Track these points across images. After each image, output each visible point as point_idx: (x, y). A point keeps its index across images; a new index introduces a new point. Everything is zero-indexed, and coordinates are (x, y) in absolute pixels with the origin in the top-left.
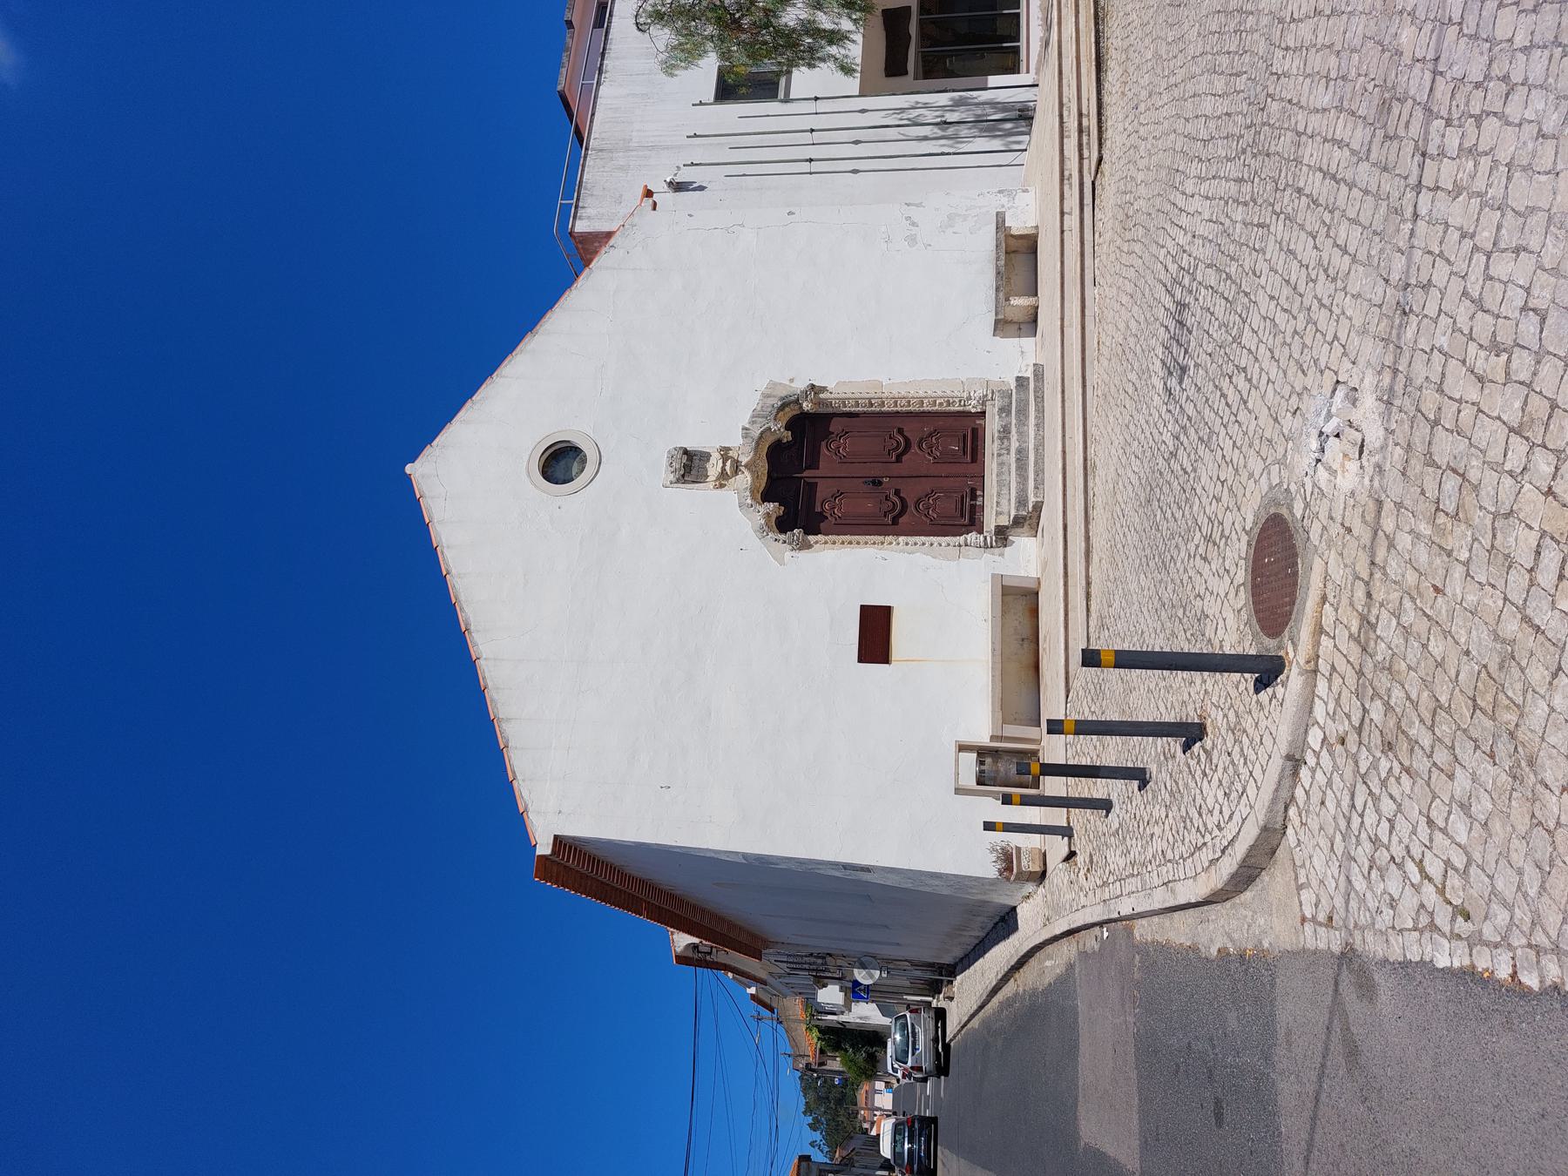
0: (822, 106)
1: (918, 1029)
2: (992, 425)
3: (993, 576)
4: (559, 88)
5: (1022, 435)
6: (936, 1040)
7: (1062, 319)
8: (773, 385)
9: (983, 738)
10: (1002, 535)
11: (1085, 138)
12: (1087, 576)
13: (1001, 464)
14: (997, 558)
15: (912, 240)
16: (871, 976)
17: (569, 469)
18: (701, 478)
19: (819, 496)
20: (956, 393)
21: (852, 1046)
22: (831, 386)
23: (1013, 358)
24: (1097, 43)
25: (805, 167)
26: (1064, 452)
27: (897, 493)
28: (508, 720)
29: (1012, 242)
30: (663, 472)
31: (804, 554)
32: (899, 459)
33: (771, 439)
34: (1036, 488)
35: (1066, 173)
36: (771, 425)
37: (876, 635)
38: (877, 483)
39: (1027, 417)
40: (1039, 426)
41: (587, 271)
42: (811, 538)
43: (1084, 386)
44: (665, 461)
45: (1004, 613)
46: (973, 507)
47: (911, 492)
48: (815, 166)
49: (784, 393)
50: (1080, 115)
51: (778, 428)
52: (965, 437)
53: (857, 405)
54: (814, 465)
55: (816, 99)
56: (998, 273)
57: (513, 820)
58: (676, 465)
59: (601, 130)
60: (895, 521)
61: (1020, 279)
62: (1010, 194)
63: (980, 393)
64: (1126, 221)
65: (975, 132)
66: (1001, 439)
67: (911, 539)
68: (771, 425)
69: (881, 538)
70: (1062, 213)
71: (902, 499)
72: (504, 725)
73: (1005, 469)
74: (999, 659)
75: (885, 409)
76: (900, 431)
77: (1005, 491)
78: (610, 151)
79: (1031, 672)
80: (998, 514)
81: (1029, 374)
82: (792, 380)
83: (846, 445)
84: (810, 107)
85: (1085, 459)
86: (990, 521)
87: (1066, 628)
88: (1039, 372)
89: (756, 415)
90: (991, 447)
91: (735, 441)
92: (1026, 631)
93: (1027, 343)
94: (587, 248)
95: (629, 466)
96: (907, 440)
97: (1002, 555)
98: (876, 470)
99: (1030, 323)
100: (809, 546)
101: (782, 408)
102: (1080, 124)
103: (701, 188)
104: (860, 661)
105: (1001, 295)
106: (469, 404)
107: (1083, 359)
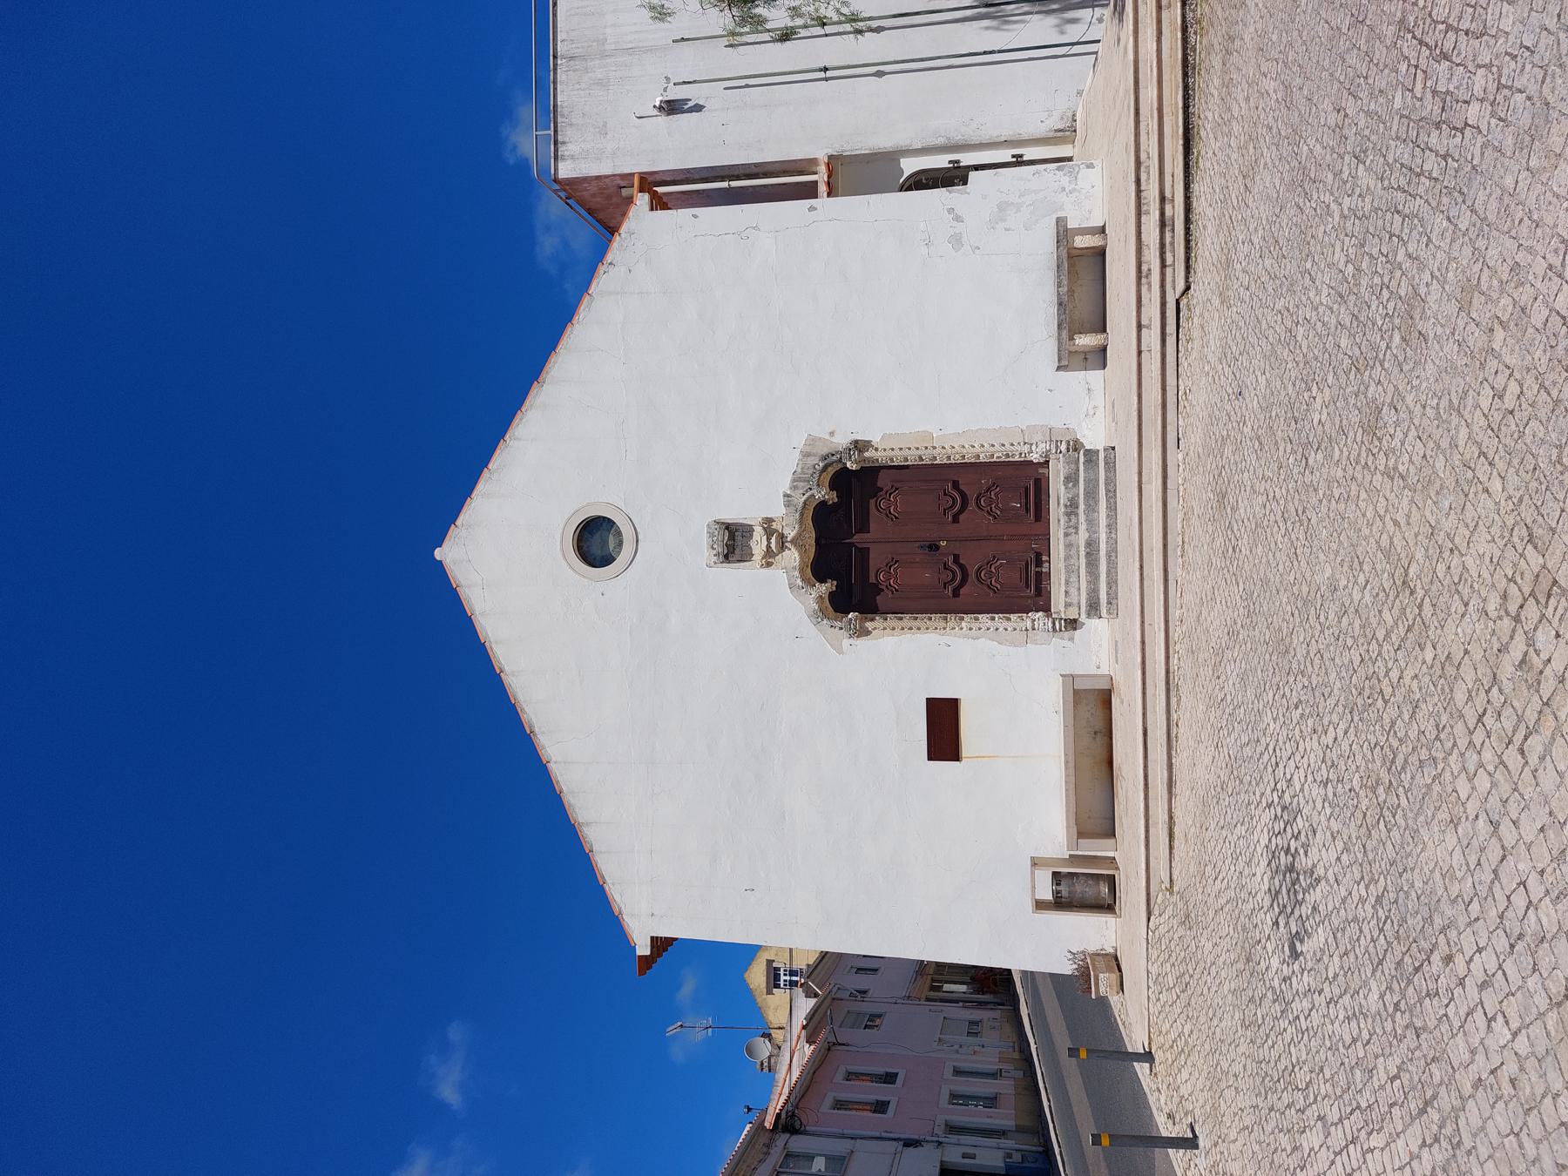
7: (1140, 474)
8: (812, 440)
11: (1168, 235)
13: (1069, 546)
18: (746, 557)
22: (875, 438)
24: (1186, 107)
26: (1143, 642)
30: (703, 549)
32: (956, 519)
34: (1109, 603)
35: (1144, 268)
37: (944, 730)
38: (933, 547)
39: (1097, 502)
40: (1112, 527)
41: (586, 299)
42: (869, 625)
46: (1039, 575)
49: (825, 451)
50: (1163, 199)
51: (823, 494)
54: (864, 528)
56: (1060, 304)
66: (1068, 514)
68: (814, 491)
70: (1139, 327)
74: (1072, 771)
76: (956, 485)
77: (1073, 579)
78: (583, 58)
79: (1104, 768)
82: (832, 434)
85: (1167, 672)
91: (778, 510)
95: (667, 542)
97: (1071, 639)
100: (868, 633)
102: (1162, 214)
103: (698, 108)
104: (928, 700)
105: (1065, 333)
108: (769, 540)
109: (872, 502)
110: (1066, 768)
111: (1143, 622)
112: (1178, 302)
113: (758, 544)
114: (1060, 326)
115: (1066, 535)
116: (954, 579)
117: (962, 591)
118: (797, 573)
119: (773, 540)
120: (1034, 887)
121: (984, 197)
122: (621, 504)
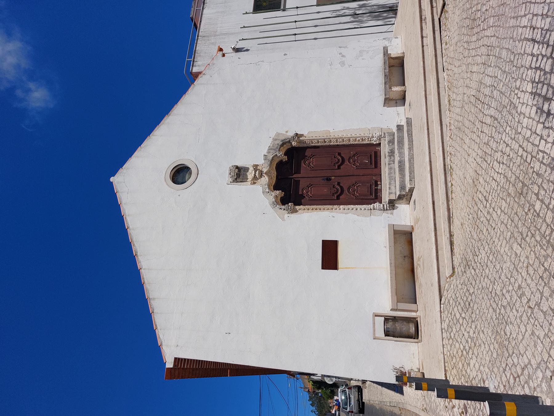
0: (300, 11)
1: (351, 396)
2: (385, 150)
3: (389, 225)
4: (191, 16)
5: (401, 154)
6: (358, 400)
7: (425, 91)
8: (278, 134)
9: (388, 312)
10: (392, 204)
12: (450, 232)
13: (390, 169)
14: (389, 215)
15: (343, 64)
16: (332, 380)
17: (184, 177)
19: (301, 187)
20: (366, 135)
21: (325, 387)
22: (305, 133)
23: (395, 117)
25: (293, 38)
26: (430, 161)
27: (339, 184)
28: (154, 299)
29: (392, 61)
30: (225, 175)
32: (339, 168)
33: (277, 160)
34: (410, 180)
35: (423, 17)
36: (277, 153)
37: (330, 255)
38: (328, 179)
39: (403, 145)
41: (193, 86)
42: (297, 207)
43: (441, 125)
45: (395, 243)
46: (376, 190)
47: (345, 183)
48: (298, 37)
49: (283, 138)
51: (281, 154)
52: (371, 156)
53: (318, 142)
54: (298, 171)
55: (297, 8)
56: (385, 76)
57: (155, 349)
58: (232, 174)
59: (204, 27)
60: (338, 198)
61: (396, 77)
62: (389, 40)
63: (378, 134)
64: (473, 23)
65: (370, 18)
66: (390, 156)
67: (346, 207)
68: (277, 153)
69: (331, 207)
70: (422, 37)
71: (341, 187)
72: (152, 302)
74: (393, 268)
75: (332, 144)
76: (339, 154)
77: (393, 182)
78: (208, 36)
80: (390, 193)
81: (403, 123)
82: (287, 132)
83: (313, 162)
84: (294, 12)
86: (386, 197)
87: (438, 259)
88: (409, 122)
89: (270, 149)
90: (384, 160)
91: (261, 161)
92: (407, 253)
93: (401, 109)
94: (196, 76)
95: (211, 175)
96: (342, 158)
97: (392, 214)
98: (327, 174)
99: (402, 100)
100: (296, 211)
101: (282, 145)
103: (247, 50)
104: (323, 241)
105: (387, 86)
106: (139, 148)
107: (440, 111)
108: (255, 172)
109: (302, 161)
110: (391, 266)
111: (430, 153)
112: (439, 19)
113: (250, 175)
114: (385, 83)
115: (389, 164)
116: (337, 192)
117: (341, 197)
118: (267, 186)
119: (257, 172)
120: (374, 331)
121: (354, 49)
122: (193, 160)
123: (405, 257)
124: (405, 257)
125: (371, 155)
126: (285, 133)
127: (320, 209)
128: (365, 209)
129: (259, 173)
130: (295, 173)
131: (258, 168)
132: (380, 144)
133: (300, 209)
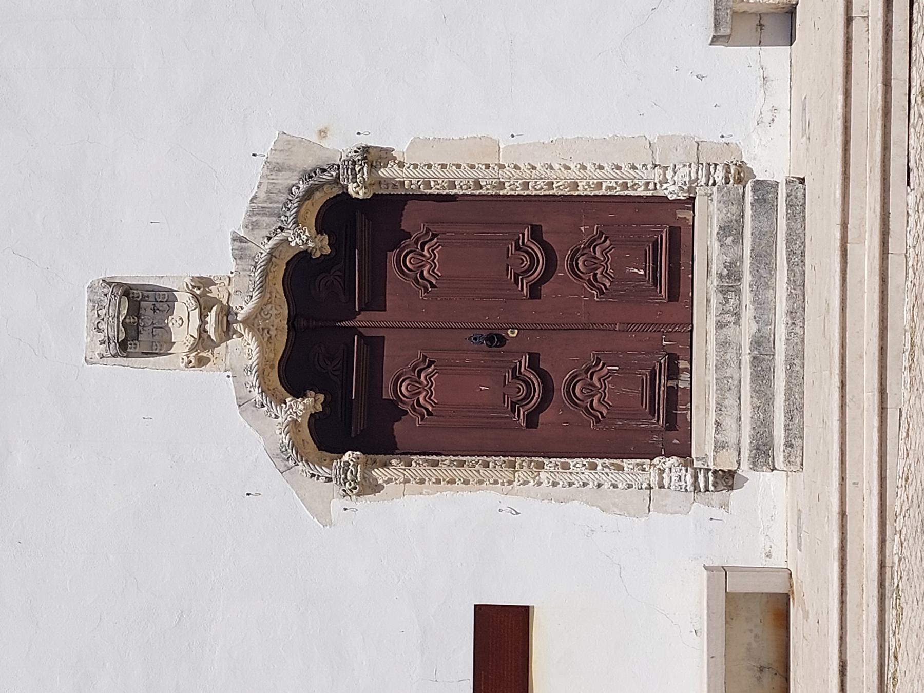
5: (763, 307)
7: (844, 225)
8: (287, 143)
13: (724, 345)
18: (160, 346)
22: (400, 147)
26: (843, 514)
30: (80, 330)
31: (366, 505)
34: (789, 445)
38: (496, 340)
39: (772, 271)
42: (379, 474)
43: (883, 409)
44: (84, 305)
46: (672, 392)
47: (561, 364)
49: (310, 163)
51: (304, 238)
52: (656, 246)
53: (452, 185)
54: (375, 300)
66: (723, 291)
68: (289, 234)
71: (544, 377)
73: (731, 355)
75: (506, 191)
77: (731, 401)
82: (323, 133)
83: (432, 260)
85: (882, 565)
89: (257, 211)
91: (220, 264)
92: (768, 655)
93: (775, 56)
97: (724, 505)
100: (376, 488)
101: (309, 194)
104: (480, 610)
108: (203, 317)
109: (392, 256)
113: (183, 324)
115: (720, 326)
118: (252, 379)
119: (211, 318)
123: (761, 669)
124: (761, 669)
125: (655, 244)
126: (314, 138)
127: (466, 482)
128: (630, 486)
129: (218, 322)
130: (364, 308)
131: (214, 292)
132: (692, 200)
133: (389, 481)
